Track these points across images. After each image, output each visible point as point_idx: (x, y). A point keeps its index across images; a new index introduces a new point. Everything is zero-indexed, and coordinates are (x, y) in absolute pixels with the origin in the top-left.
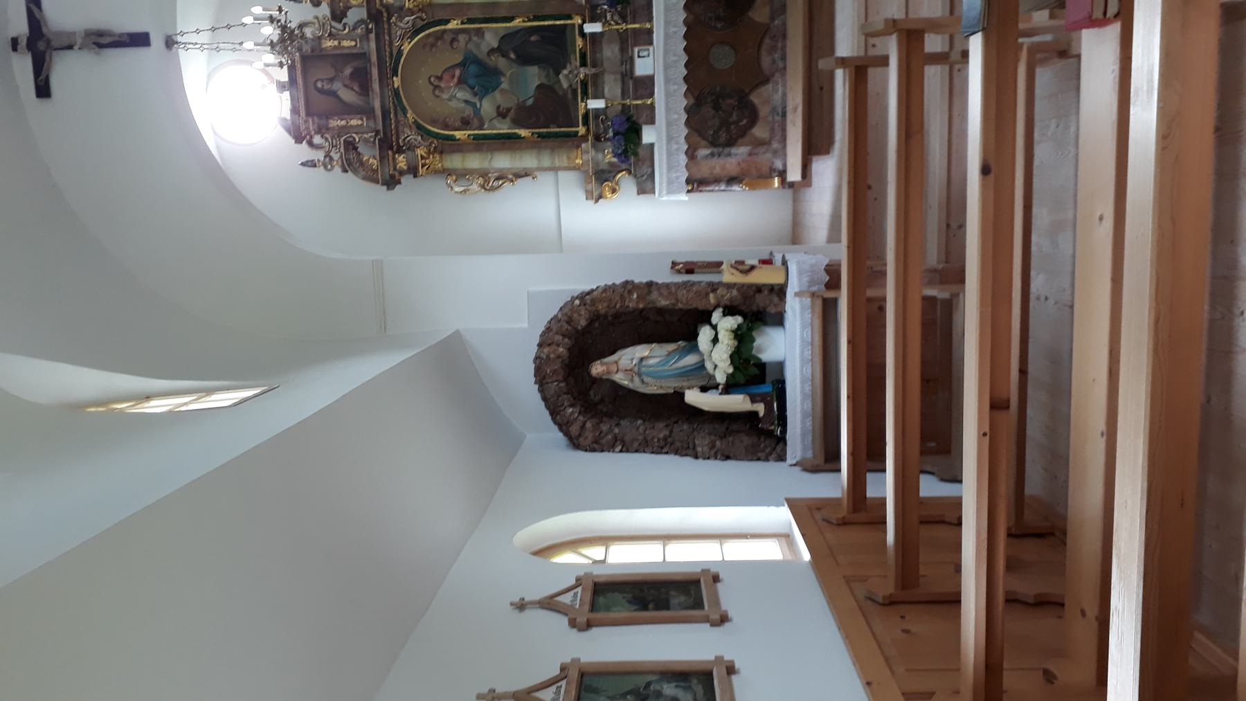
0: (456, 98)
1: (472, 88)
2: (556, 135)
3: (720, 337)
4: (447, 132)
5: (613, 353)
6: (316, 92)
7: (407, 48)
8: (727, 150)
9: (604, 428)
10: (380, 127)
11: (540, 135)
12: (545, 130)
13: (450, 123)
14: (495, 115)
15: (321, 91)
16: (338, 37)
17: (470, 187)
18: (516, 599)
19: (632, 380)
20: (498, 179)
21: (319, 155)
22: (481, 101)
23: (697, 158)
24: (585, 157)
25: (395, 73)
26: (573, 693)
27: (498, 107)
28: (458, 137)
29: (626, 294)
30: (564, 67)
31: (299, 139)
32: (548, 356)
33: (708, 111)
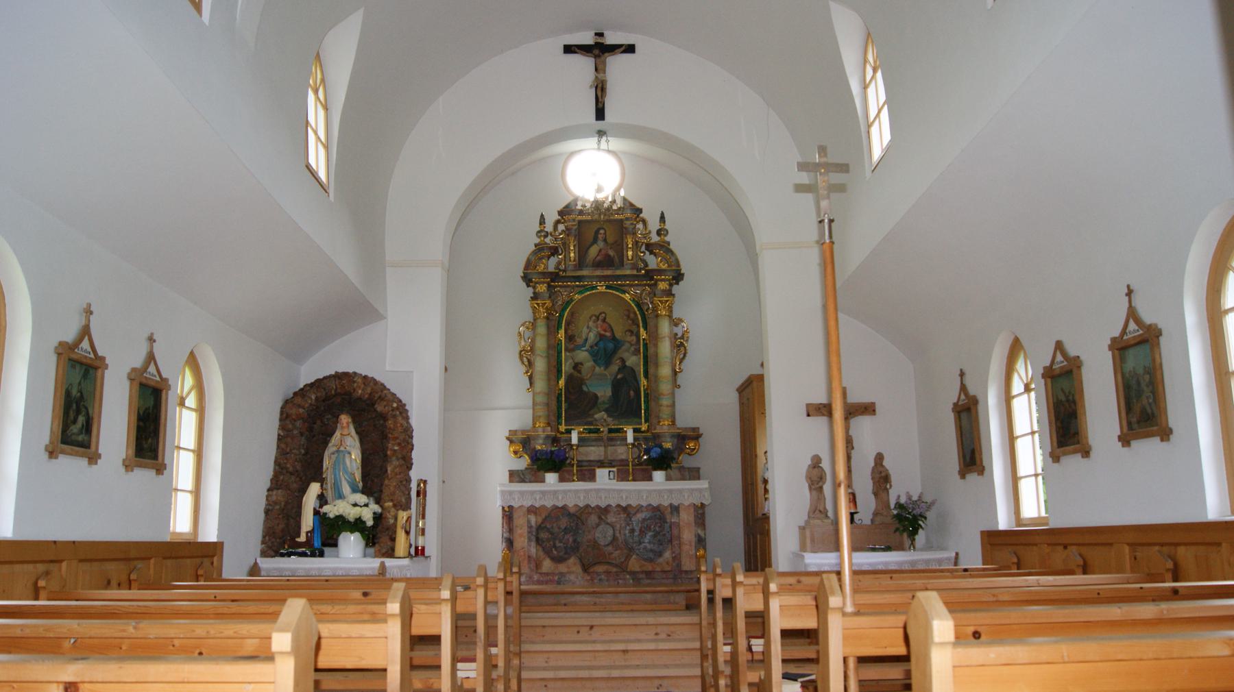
0: (589, 332)
1: (596, 345)
2: (559, 407)
3: (358, 508)
4: (563, 325)
5: (357, 433)
6: (596, 229)
7: (627, 297)
8: (534, 538)
9: (298, 423)
10: (569, 274)
11: (560, 395)
12: (563, 399)
13: (570, 326)
14: (576, 361)
15: (597, 232)
16: (635, 247)
17: (523, 339)
18: (155, 337)
19: (333, 446)
20: (529, 361)
21: (549, 227)
22: (586, 351)
24: (540, 429)
25: (607, 287)
26: (85, 361)
27: (581, 364)
28: (560, 331)
29: (398, 441)
30: (609, 416)
31: (561, 213)
32: (354, 382)
33: (564, 522)
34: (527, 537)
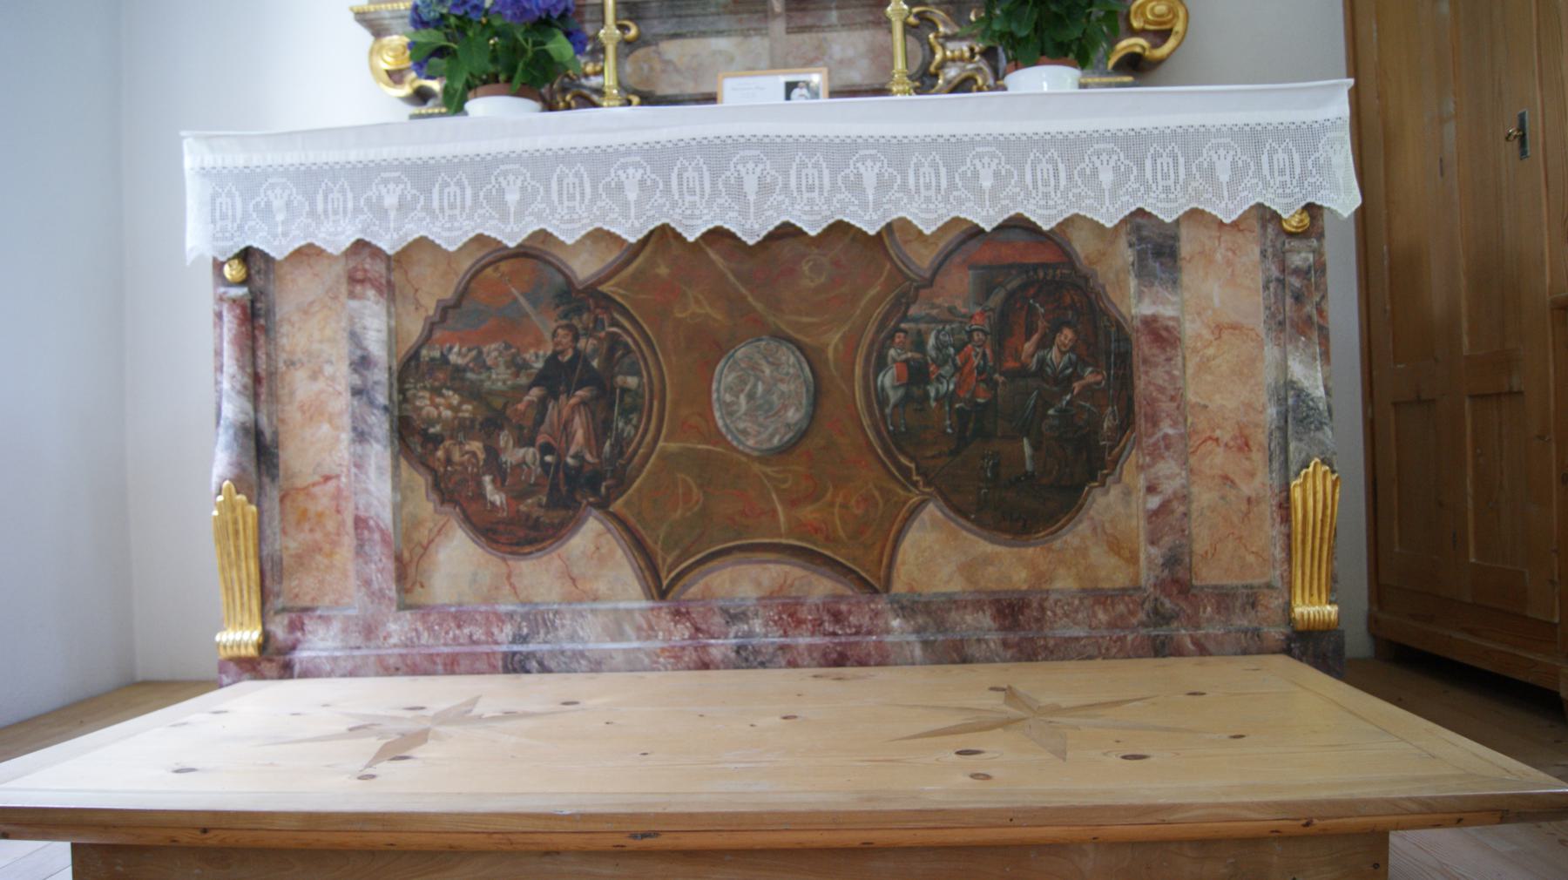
8: (380, 424)
23: (352, 295)
34: (346, 421)
